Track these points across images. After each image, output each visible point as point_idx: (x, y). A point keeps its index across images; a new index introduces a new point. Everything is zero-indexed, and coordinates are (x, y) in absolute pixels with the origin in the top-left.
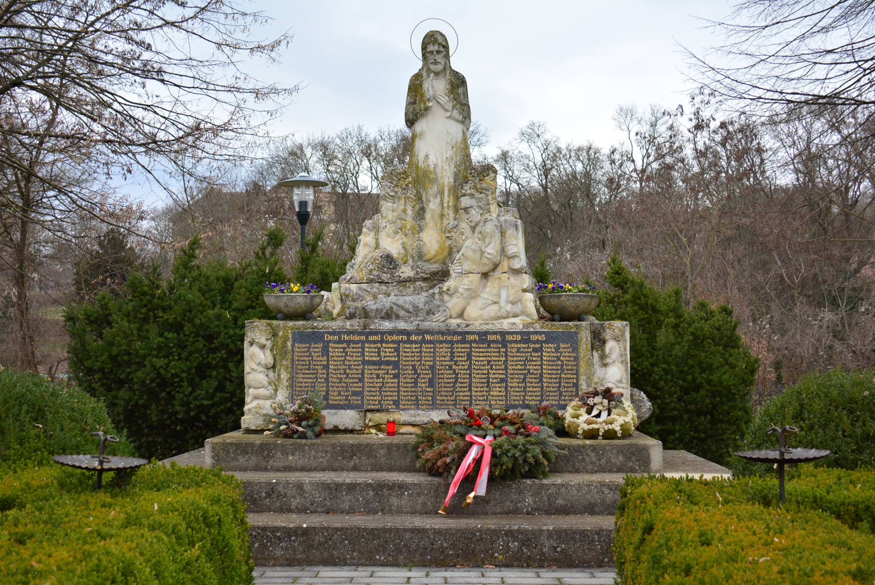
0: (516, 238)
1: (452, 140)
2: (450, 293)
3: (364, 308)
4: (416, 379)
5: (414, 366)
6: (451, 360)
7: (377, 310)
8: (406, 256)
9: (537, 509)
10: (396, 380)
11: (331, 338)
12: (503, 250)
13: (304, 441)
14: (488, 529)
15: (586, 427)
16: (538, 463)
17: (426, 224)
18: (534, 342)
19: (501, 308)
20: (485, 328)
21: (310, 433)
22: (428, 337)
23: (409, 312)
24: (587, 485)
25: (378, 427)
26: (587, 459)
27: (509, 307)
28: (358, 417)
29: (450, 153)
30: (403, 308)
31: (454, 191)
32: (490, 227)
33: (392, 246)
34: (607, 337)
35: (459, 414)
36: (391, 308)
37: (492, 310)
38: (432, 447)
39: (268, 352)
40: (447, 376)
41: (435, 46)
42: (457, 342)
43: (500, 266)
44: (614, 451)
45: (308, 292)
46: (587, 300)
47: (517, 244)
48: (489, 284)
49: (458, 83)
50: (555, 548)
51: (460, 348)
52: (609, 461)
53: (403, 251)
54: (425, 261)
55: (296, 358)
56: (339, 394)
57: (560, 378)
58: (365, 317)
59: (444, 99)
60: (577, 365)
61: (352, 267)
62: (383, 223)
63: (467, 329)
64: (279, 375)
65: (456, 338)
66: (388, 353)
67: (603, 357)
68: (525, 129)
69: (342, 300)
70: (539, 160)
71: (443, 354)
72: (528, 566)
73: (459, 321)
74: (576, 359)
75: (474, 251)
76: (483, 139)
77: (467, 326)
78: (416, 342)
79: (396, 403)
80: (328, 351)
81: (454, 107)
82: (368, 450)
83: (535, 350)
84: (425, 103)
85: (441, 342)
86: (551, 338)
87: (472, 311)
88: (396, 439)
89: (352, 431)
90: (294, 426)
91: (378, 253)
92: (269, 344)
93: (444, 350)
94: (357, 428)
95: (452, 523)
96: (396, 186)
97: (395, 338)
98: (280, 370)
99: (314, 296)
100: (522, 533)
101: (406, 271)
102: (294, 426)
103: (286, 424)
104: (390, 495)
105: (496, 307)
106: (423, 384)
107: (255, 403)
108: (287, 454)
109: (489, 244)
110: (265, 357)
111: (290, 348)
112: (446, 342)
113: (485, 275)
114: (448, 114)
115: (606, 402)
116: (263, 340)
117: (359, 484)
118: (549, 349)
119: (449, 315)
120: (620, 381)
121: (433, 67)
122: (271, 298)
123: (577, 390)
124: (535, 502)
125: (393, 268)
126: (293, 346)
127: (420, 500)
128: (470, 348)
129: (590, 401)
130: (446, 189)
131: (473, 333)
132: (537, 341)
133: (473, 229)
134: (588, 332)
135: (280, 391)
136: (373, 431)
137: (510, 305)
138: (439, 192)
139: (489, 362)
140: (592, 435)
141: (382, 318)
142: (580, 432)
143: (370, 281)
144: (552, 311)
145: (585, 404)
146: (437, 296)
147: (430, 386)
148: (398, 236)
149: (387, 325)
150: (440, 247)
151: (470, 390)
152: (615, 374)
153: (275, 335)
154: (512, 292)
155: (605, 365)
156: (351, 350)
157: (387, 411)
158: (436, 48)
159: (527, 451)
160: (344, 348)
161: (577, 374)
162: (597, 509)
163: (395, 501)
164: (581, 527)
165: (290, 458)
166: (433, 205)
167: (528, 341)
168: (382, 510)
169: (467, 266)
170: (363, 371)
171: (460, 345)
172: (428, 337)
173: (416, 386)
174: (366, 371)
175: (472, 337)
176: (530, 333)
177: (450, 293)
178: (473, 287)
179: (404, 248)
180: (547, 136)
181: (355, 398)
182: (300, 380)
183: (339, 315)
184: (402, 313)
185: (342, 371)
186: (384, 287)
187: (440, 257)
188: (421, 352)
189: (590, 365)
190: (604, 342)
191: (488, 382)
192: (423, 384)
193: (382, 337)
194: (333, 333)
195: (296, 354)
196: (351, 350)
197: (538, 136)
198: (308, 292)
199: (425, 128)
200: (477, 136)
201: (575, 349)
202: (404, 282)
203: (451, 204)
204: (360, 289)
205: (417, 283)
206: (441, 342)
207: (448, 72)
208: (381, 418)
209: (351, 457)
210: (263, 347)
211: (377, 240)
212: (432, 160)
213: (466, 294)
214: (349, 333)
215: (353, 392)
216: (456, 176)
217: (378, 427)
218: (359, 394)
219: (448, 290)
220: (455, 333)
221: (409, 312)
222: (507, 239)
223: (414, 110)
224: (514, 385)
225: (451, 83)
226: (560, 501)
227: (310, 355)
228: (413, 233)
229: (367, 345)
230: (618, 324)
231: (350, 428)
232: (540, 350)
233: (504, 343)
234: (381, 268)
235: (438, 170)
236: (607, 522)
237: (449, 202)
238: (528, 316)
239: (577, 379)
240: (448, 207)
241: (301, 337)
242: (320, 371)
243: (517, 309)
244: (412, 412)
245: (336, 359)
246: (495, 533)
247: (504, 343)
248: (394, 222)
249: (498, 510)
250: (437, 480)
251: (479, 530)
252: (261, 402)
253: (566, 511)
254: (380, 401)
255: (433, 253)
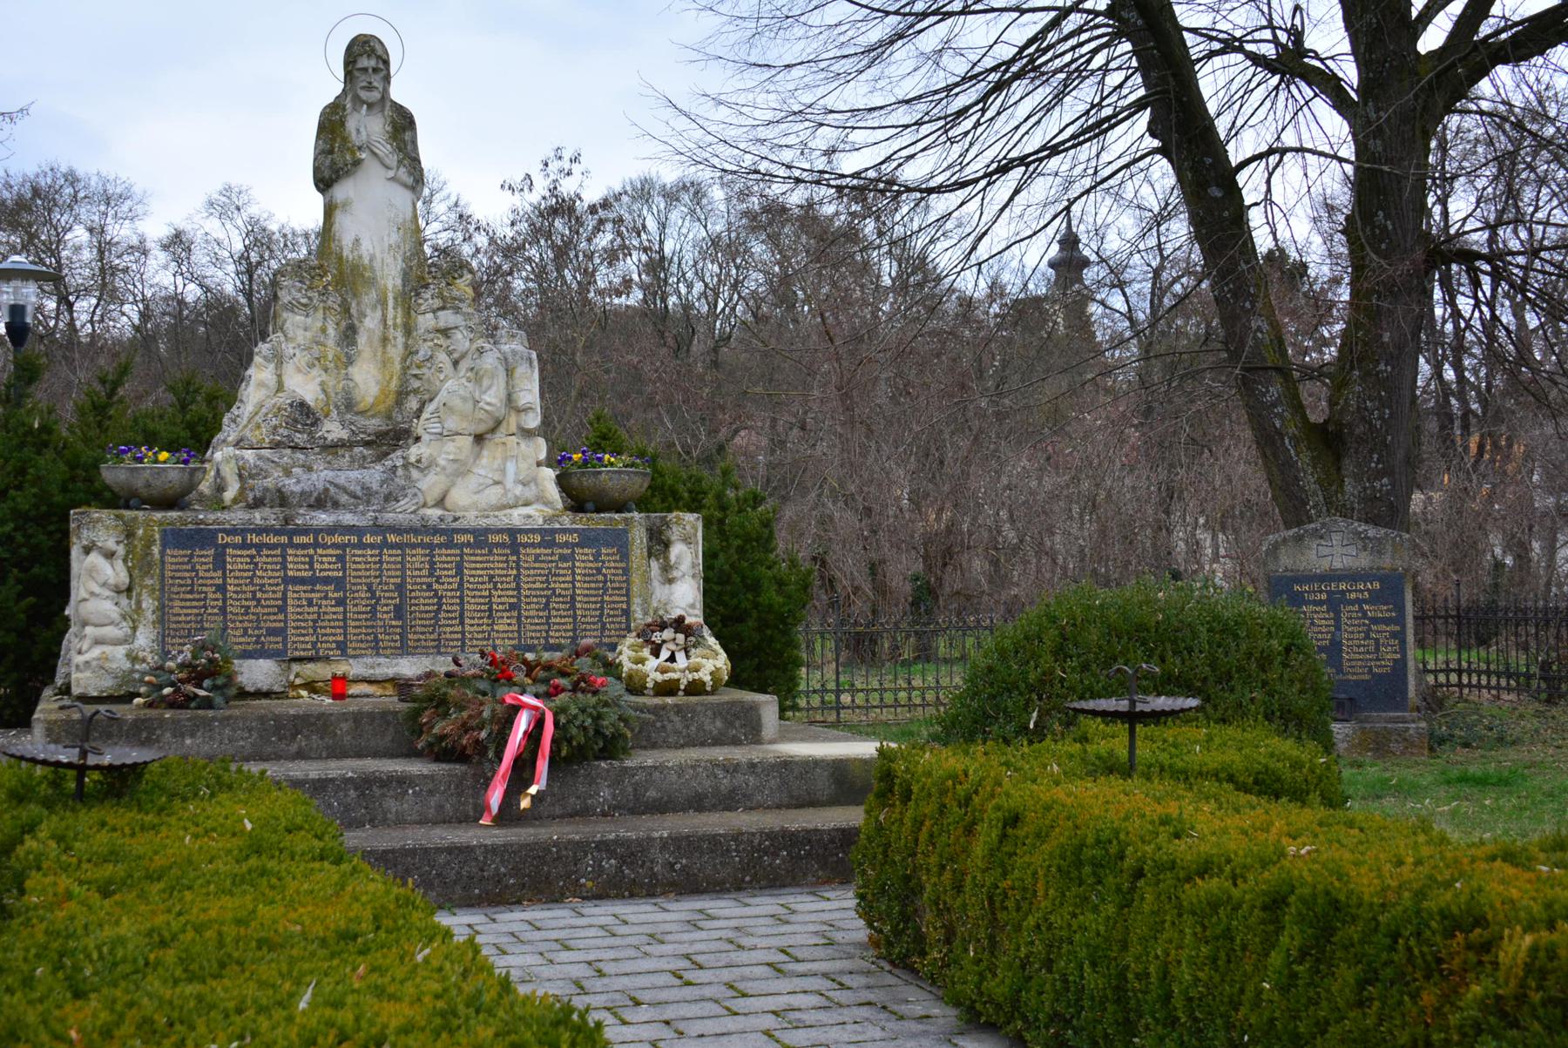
0: (530, 379)
1: (397, 216)
2: (421, 466)
3: (279, 491)
4: (374, 607)
5: (369, 586)
6: (431, 575)
7: (303, 493)
8: (327, 404)
9: (616, 808)
10: (341, 609)
11: (228, 539)
12: (510, 399)
13: (210, 713)
14: (570, 842)
15: (659, 677)
16: (618, 736)
17: (359, 352)
18: (561, 546)
19: (506, 491)
20: (484, 523)
21: (219, 700)
22: (392, 538)
23: (356, 497)
24: (692, 767)
25: (311, 686)
26: (669, 727)
27: (518, 490)
28: (278, 670)
29: (395, 238)
30: (345, 490)
31: (404, 300)
32: (490, 360)
33: (306, 387)
34: (673, 538)
35: (472, 661)
36: (326, 490)
37: (493, 495)
38: (446, 715)
39: (119, 564)
40: (424, 601)
41: (365, 60)
42: (440, 546)
43: (504, 424)
44: (709, 713)
45: (186, 462)
46: (638, 480)
47: (530, 391)
48: (485, 453)
49: (403, 124)
50: (672, 865)
51: (444, 556)
52: (700, 728)
53: (322, 396)
54: (357, 413)
55: (168, 574)
56: (245, 634)
57: (602, 602)
58: (281, 506)
59: (385, 149)
60: (627, 581)
61: (234, 421)
62: (288, 349)
63: (455, 525)
64: (139, 603)
65: (437, 540)
66: (326, 564)
67: (666, 568)
68: (216, 196)
69: (240, 476)
70: (238, 246)
71: (417, 565)
72: (632, 896)
73: (438, 512)
74: (626, 571)
75: (464, 399)
76: (139, 209)
77: (456, 519)
78: (372, 546)
79: (342, 647)
80: (224, 562)
81: (400, 162)
82: (303, 723)
83: (563, 558)
84: (353, 153)
85: (414, 546)
86: (587, 539)
87: (461, 496)
88: (351, 706)
89: (267, 694)
90: (190, 688)
91: (283, 400)
92: (121, 550)
93: (419, 558)
94: (276, 688)
95: (501, 836)
96: (310, 288)
97: (337, 539)
98: (139, 595)
99: (196, 469)
100: (622, 845)
101: (333, 430)
102: (190, 688)
103: (172, 684)
104: (384, 795)
105: (498, 490)
106: (385, 614)
107: (96, 652)
108: (183, 736)
109: (489, 388)
110: (115, 573)
111: (157, 556)
112: (422, 545)
113: (479, 439)
114: (391, 174)
115: (681, 637)
116: (111, 544)
117: (332, 780)
118: (584, 555)
119: (421, 502)
120: (693, 606)
121: (364, 95)
122: (114, 474)
123: (628, 620)
124: (614, 796)
125: (312, 425)
126: (162, 553)
127: (433, 801)
128: (461, 556)
129: (657, 637)
130: (390, 296)
131: (465, 531)
132: (566, 545)
133: (456, 363)
134: (643, 530)
135: (141, 629)
136: (304, 693)
137: (520, 487)
138: (379, 301)
139: (491, 577)
140: (667, 689)
141: (310, 506)
142: (650, 685)
143: (276, 446)
144: (577, 500)
145: (648, 642)
146: (400, 472)
147: (397, 618)
148: (315, 372)
149: (323, 518)
150: (382, 391)
151: (462, 623)
152: (684, 596)
153: (130, 535)
154: (523, 466)
155: (671, 581)
156: (264, 559)
157: (327, 659)
158: (372, 63)
159: (599, 717)
160: (252, 557)
161: (627, 595)
162: (707, 803)
163: (392, 805)
164: (709, 830)
165: (188, 742)
166: (370, 323)
167: (551, 544)
168: (371, 821)
169: (452, 423)
170: (285, 593)
171: (444, 551)
172: (392, 538)
173: (374, 617)
174: (290, 594)
175: (462, 538)
176: (554, 531)
177: (421, 466)
178: (462, 457)
179: (324, 391)
180: (253, 210)
181: (272, 639)
182: (176, 610)
183: (235, 501)
184: (344, 498)
185: (249, 595)
186: (300, 456)
187: (382, 408)
188: (380, 562)
189: (647, 580)
190: (667, 545)
191: (490, 610)
192: (385, 614)
193: (316, 539)
194: (232, 532)
195: (168, 567)
196: (264, 559)
197: (238, 209)
198: (186, 462)
199: (351, 194)
200: (128, 203)
201: (625, 556)
202: (332, 448)
203: (399, 321)
204: (260, 458)
205: (357, 450)
206: (414, 546)
207: (388, 104)
208: (321, 671)
209: (294, 736)
210: (109, 555)
211: (279, 376)
212: (366, 248)
213: (451, 468)
214: (260, 531)
215: (268, 629)
216: (405, 275)
217: (311, 686)
218: (280, 632)
219: (419, 461)
220: (436, 531)
221: (356, 497)
222: (517, 382)
223: (333, 162)
224: (532, 613)
225: (393, 123)
226: (652, 794)
227: (193, 569)
228: (337, 367)
229: (290, 551)
230: (690, 517)
231: (265, 688)
232: (572, 558)
233: (515, 547)
234: (292, 423)
235: (377, 264)
236: (851, 816)
237: (395, 318)
238: (547, 503)
239: (628, 603)
240: (395, 325)
241: (175, 538)
242: (210, 596)
243: (530, 493)
244: (369, 660)
245: (237, 574)
246: (582, 847)
247: (515, 547)
248: (308, 349)
249: (558, 810)
250: (459, 768)
251: (556, 844)
252: (107, 649)
253: (661, 807)
254: (314, 644)
255: (370, 400)
